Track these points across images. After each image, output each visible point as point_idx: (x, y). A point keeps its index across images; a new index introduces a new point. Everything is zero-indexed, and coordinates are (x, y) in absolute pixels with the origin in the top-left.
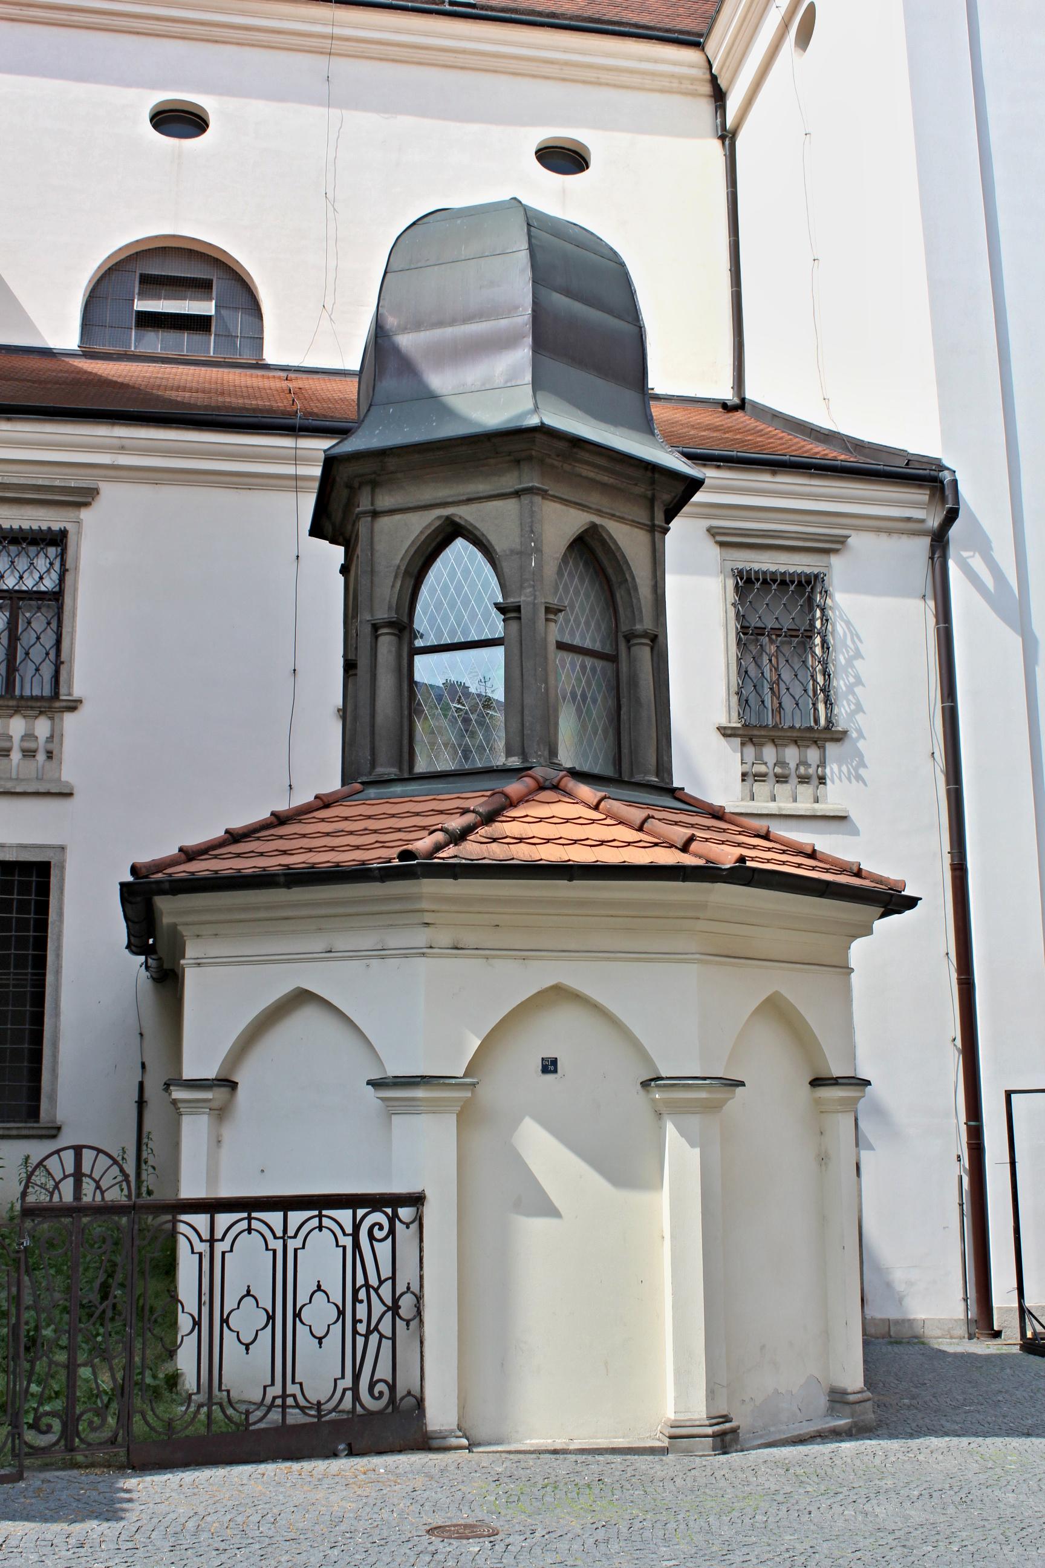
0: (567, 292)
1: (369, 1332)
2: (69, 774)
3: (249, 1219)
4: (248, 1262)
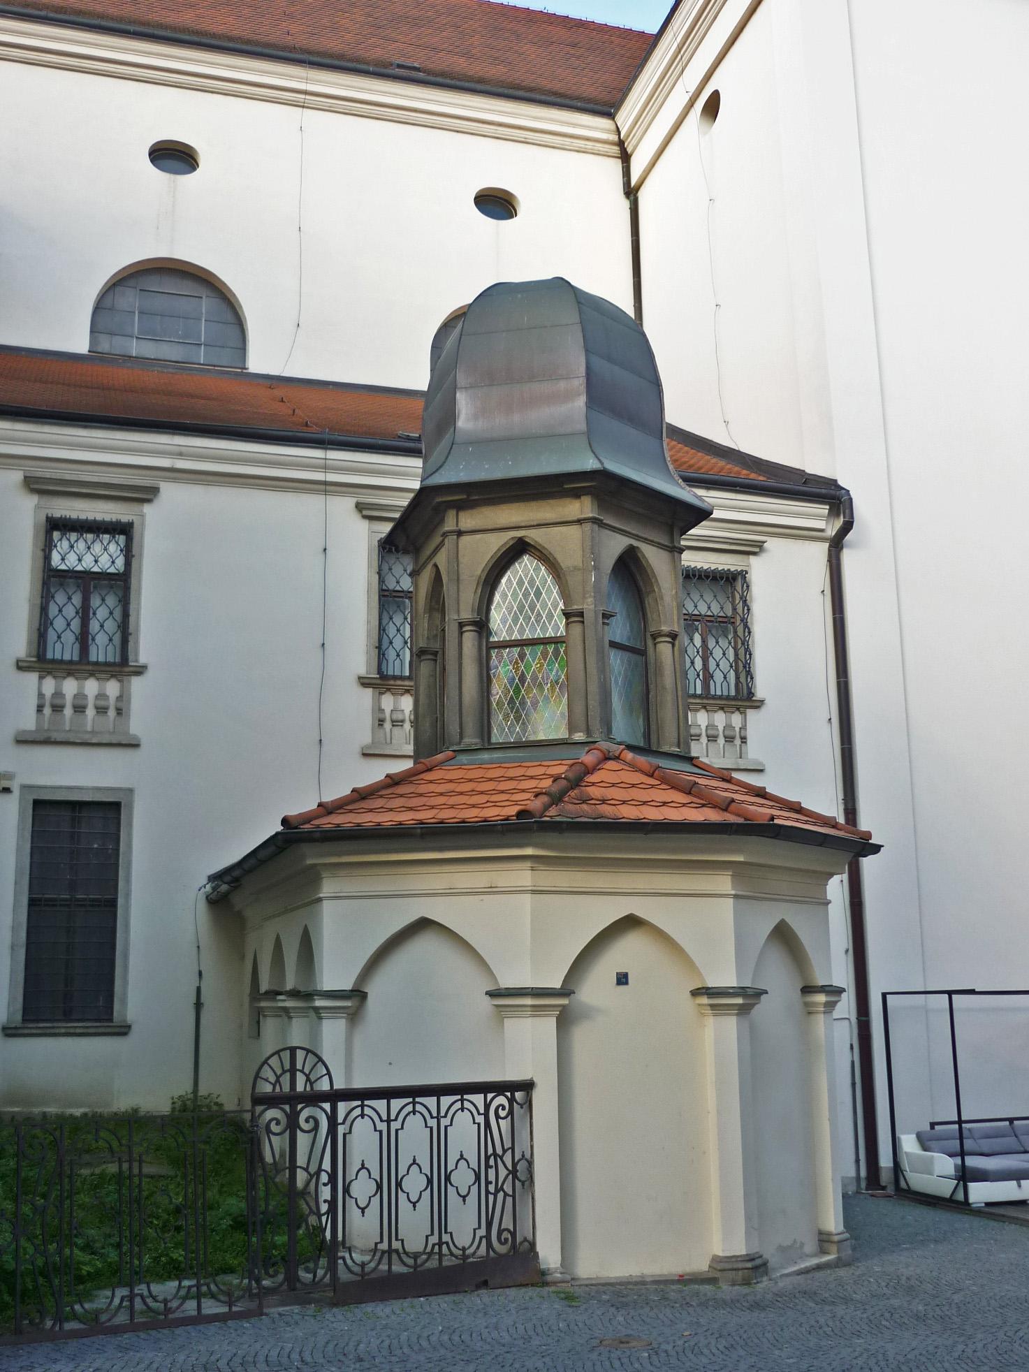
0: (610, 359)
1: (497, 1191)
2: (136, 726)
3: (362, 1106)
4: (362, 1140)
